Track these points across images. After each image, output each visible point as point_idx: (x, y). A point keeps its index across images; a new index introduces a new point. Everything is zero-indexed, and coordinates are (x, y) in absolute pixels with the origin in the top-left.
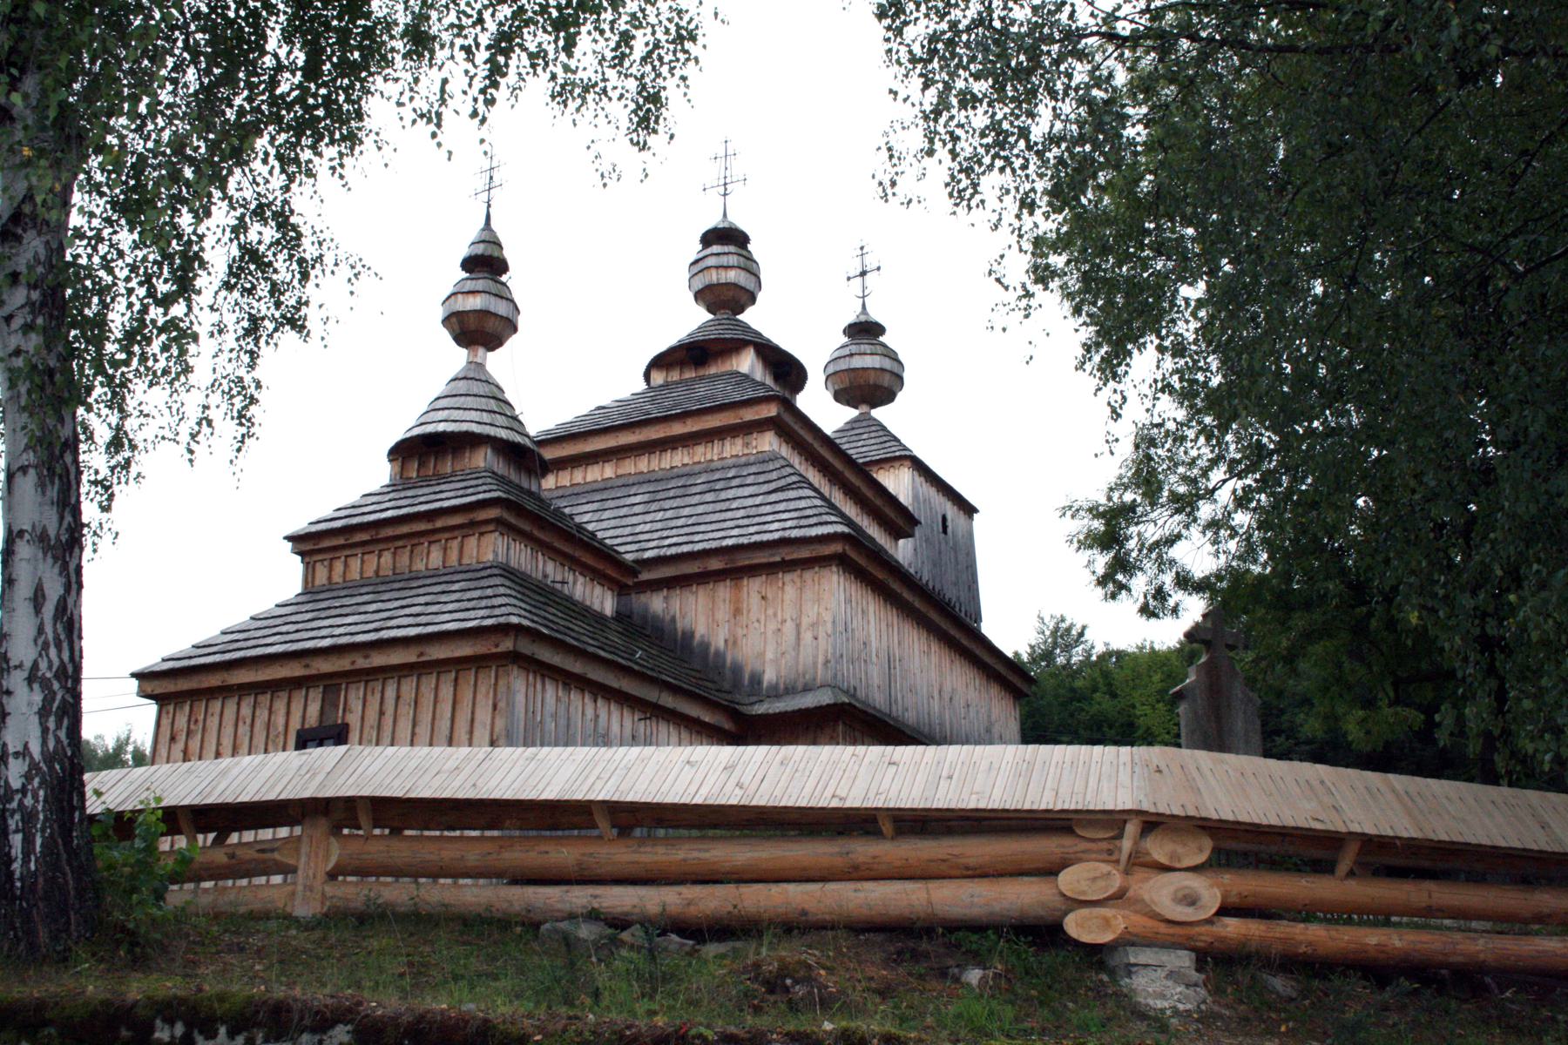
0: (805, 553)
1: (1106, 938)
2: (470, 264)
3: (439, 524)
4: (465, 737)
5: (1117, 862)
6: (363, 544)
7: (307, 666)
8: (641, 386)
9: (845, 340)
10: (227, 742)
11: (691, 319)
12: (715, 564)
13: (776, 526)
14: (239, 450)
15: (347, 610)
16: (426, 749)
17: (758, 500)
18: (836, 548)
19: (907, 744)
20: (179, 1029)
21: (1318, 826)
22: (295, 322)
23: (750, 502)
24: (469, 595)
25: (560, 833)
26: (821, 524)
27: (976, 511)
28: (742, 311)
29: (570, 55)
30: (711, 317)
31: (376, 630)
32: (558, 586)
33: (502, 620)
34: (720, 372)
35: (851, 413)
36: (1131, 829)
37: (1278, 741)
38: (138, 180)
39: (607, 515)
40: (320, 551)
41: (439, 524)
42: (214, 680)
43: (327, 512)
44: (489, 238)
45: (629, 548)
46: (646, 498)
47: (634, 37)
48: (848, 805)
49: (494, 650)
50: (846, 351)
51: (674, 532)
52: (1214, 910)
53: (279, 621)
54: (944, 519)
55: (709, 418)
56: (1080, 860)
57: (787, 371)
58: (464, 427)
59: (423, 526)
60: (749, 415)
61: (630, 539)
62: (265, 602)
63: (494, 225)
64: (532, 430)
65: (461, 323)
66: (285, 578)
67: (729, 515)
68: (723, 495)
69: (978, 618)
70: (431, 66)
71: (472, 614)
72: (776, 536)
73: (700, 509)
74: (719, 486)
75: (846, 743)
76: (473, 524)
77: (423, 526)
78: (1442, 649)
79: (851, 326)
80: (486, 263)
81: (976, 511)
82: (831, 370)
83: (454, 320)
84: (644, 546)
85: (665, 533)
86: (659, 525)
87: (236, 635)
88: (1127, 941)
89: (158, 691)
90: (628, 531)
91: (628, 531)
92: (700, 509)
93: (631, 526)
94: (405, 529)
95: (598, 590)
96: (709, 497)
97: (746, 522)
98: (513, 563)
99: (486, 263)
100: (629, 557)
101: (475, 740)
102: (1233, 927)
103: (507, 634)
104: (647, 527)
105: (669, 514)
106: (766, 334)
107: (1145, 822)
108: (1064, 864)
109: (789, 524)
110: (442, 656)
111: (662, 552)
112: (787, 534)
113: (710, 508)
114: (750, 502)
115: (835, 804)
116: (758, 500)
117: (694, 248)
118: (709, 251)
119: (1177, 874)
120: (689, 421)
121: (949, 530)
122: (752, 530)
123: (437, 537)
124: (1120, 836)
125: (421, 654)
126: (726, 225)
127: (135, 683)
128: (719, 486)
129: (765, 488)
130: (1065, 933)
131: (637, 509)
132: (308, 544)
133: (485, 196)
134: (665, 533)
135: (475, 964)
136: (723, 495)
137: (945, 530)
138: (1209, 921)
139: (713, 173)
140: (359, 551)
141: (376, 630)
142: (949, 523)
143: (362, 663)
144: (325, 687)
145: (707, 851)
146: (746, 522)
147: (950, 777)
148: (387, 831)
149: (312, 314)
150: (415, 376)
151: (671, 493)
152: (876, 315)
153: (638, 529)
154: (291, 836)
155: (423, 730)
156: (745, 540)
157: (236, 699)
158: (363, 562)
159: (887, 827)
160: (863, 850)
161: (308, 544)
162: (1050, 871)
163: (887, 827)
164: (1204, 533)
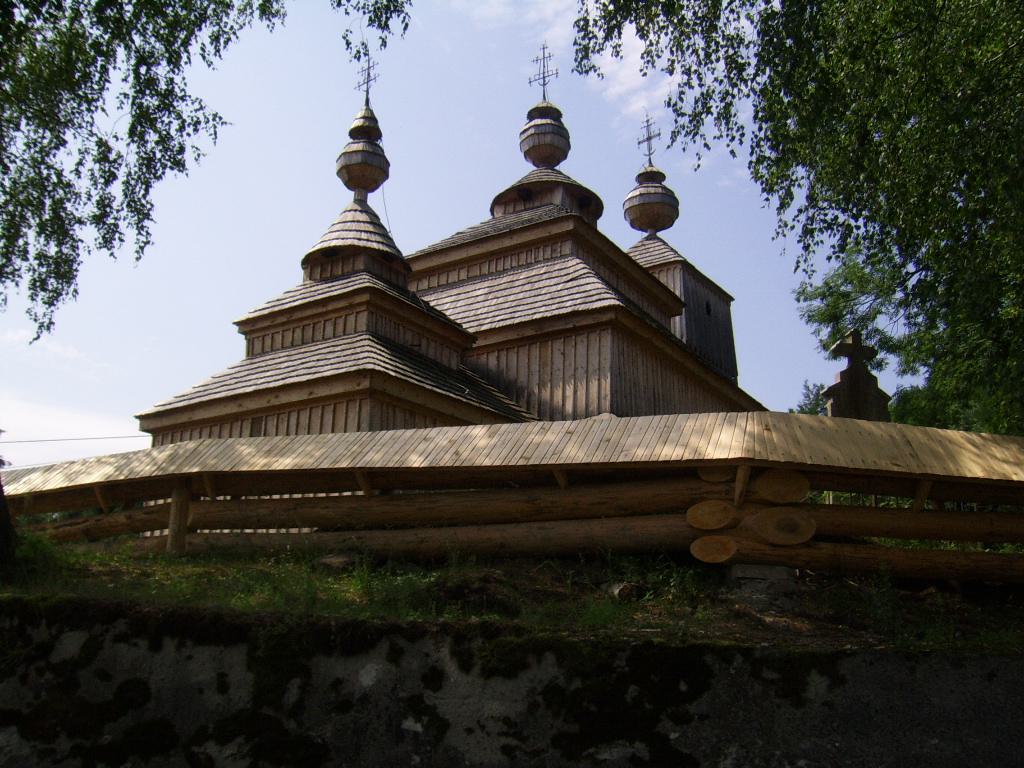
0: (589, 321)
1: (723, 558)
2: (355, 134)
3: (330, 308)
4: (238, 433)
5: (733, 500)
6: (283, 324)
7: (240, 405)
8: (488, 217)
9: (636, 184)
10: (293, 428)
11: (521, 170)
12: (530, 332)
13: (568, 304)
14: (138, 259)
15: (269, 368)
16: (331, 435)
17: (560, 287)
18: (610, 316)
19: (452, 425)
20: (16, 622)
21: (896, 469)
22: (179, 165)
23: (554, 288)
24: (345, 353)
25: (452, 491)
26: (600, 300)
27: (732, 299)
28: (558, 163)
29: (620, 38)
30: (535, 168)
31: (283, 379)
32: (416, 348)
33: (361, 367)
34: (546, 210)
35: (641, 235)
36: (741, 475)
37: (542, 118)
38: (171, 33)
39: (460, 304)
40: (327, 313)
41: (330, 308)
42: (183, 418)
43: (187, 389)
44: (370, 118)
45: (472, 324)
46: (486, 291)
47: (612, 39)
48: (531, 462)
49: (357, 388)
50: (245, 363)
51: (503, 312)
52: (810, 536)
53: (228, 377)
54: (708, 306)
55: (567, 403)
56: (702, 499)
57: (588, 204)
58: (349, 242)
59: (321, 310)
60: (556, 230)
61: (473, 318)
62: (222, 368)
63: (373, 106)
64: (404, 255)
65: (348, 173)
66: (236, 347)
67: (540, 298)
68: (536, 285)
69: (735, 374)
70: (709, 87)
71: (344, 365)
72: (569, 310)
73: (521, 296)
74: (534, 279)
75: (406, 426)
76: (351, 306)
77: (321, 310)
78: (394, 574)
79: (640, 175)
80: (368, 131)
81: (732, 299)
82: (627, 206)
83: (344, 171)
84: (482, 322)
85: (497, 313)
86: (493, 308)
87: (220, 381)
88: (741, 559)
89: (151, 427)
90: (472, 313)
91: (472, 313)
92: (521, 296)
93: (471, 306)
94: (309, 312)
95: (446, 352)
96: (527, 287)
97: (550, 302)
98: (556, 144)
99: (368, 131)
100: (471, 330)
101: (336, 430)
102: (826, 549)
103: (365, 377)
104: (486, 310)
105: (501, 300)
106: (574, 178)
107: (753, 468)
108: (692, 502)
109: (578, 301)
110: (323, 394)
111: (493, 326)
112: (576, 308)
113: (528, 294)
114: (554, 288)
115: (522, 462)
116: (560, 287)
117: (523, 123)
118: (532, 123)
119: (370, 96)
120: (515, 237)
121: (712, 312)
122: (554, 307)
123: (330, 316)
124: (733, 480)
125: (311, 393)
126: (545, 105)
127: (138, 422)
128: (534, 279)
129: (565, 279)
130: (692, 555)
131: (479, 299)
132: (248, 327)
133: (364, 87)
134: (497, 313)
135: (427, 625)
136: (536, 285)
137: (709, 312)
138: (807, 545)
139: (533, 70)
140: (280, 329)
141: (283, 379)
142: (712, 308)
143: (275, 402)
144: (253, 419)
145: (282, 453)
146: (550, 302)
147: (609, 440)
148: (228, 498)
149: (189, 157)
150: (326, 214)
151: (503, 287)
152: (554, 102)
153: (479, 312)
154: (165, 503)
155: (341, 422)
156: (549, 314)
157: (586, 335)
158: (283, 337)
159: (561, 481)
160: (546, 498)
161: (248, 327)
162: (680, 509)
163: (561, 481)
164: (120, 156)
